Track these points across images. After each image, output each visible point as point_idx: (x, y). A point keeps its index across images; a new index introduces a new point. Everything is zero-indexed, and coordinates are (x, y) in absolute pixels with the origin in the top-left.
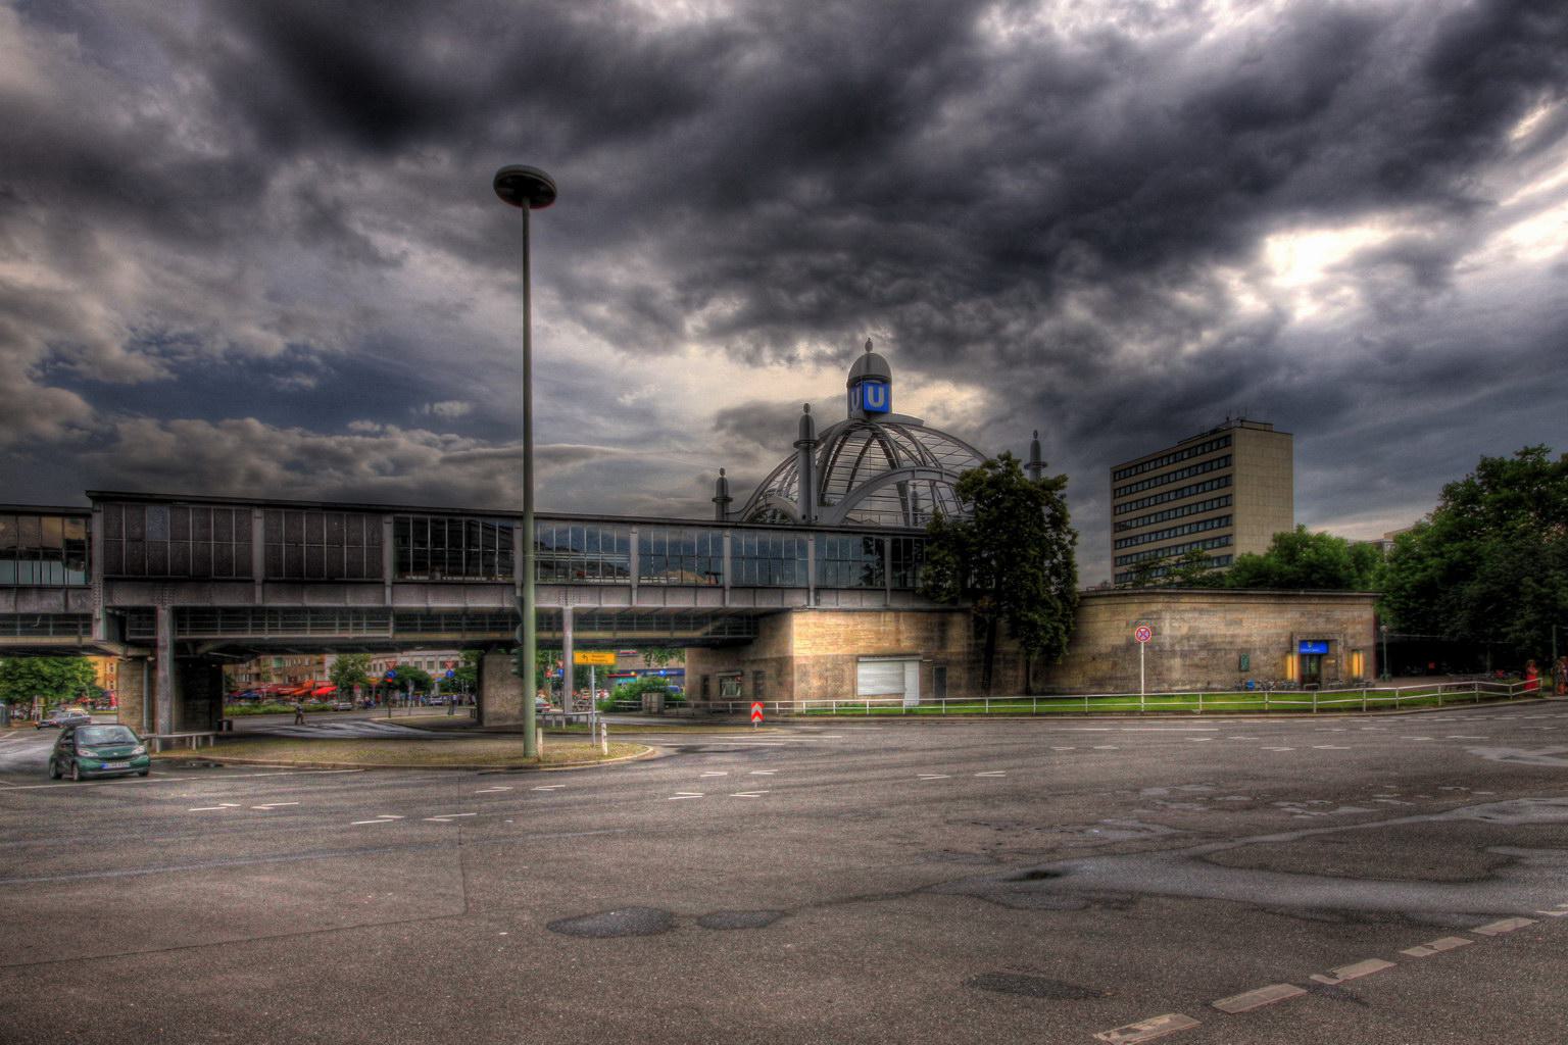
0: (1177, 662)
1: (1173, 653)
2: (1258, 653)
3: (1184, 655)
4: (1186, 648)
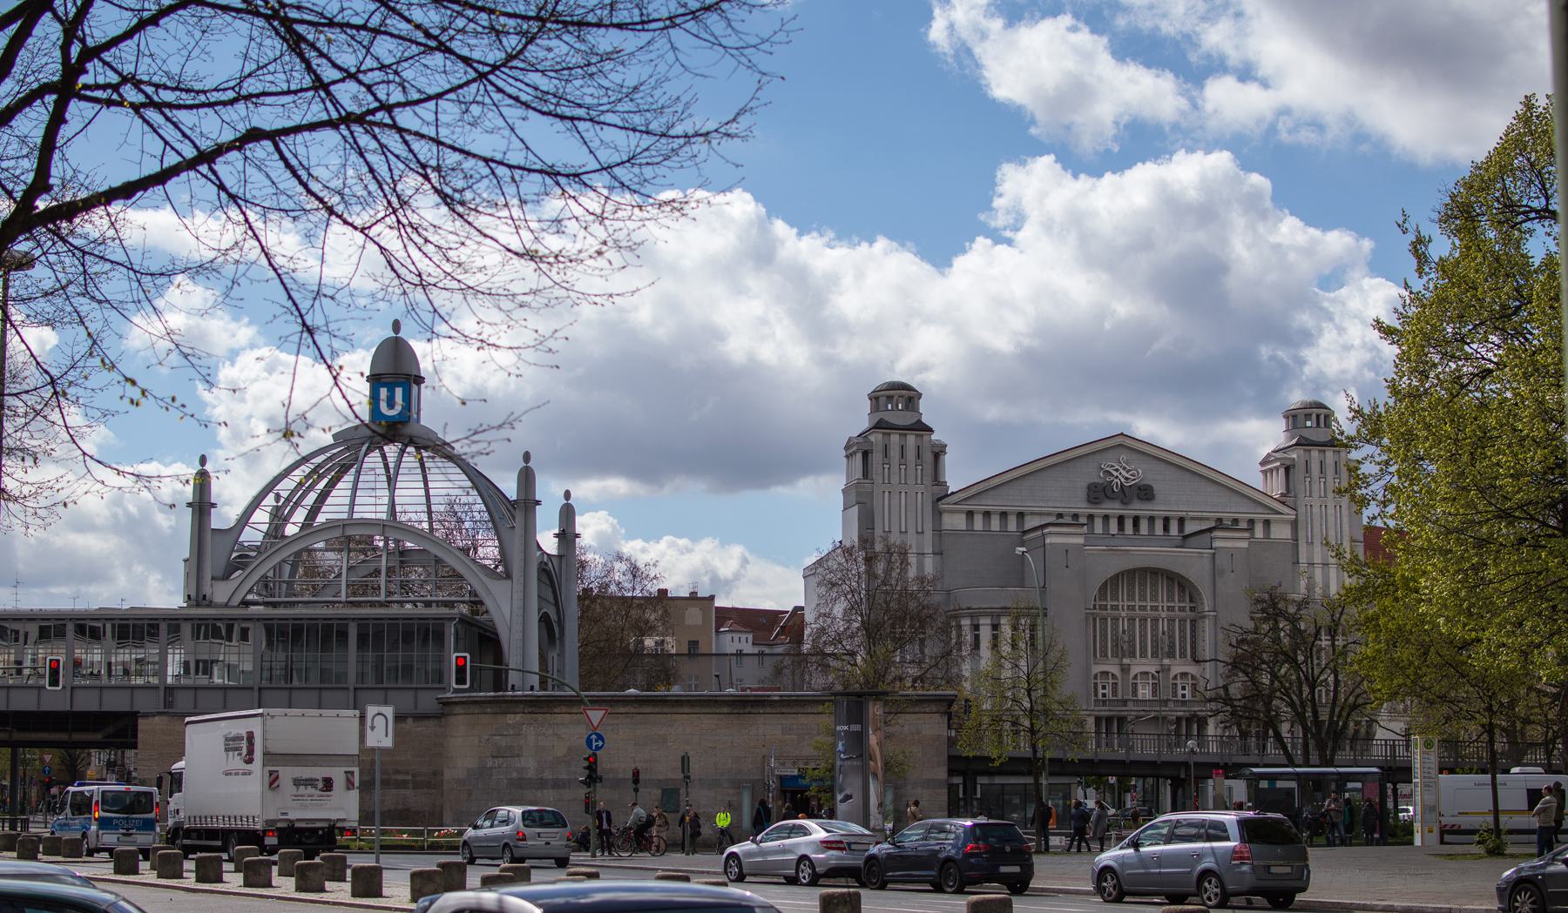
4: (564, 776)
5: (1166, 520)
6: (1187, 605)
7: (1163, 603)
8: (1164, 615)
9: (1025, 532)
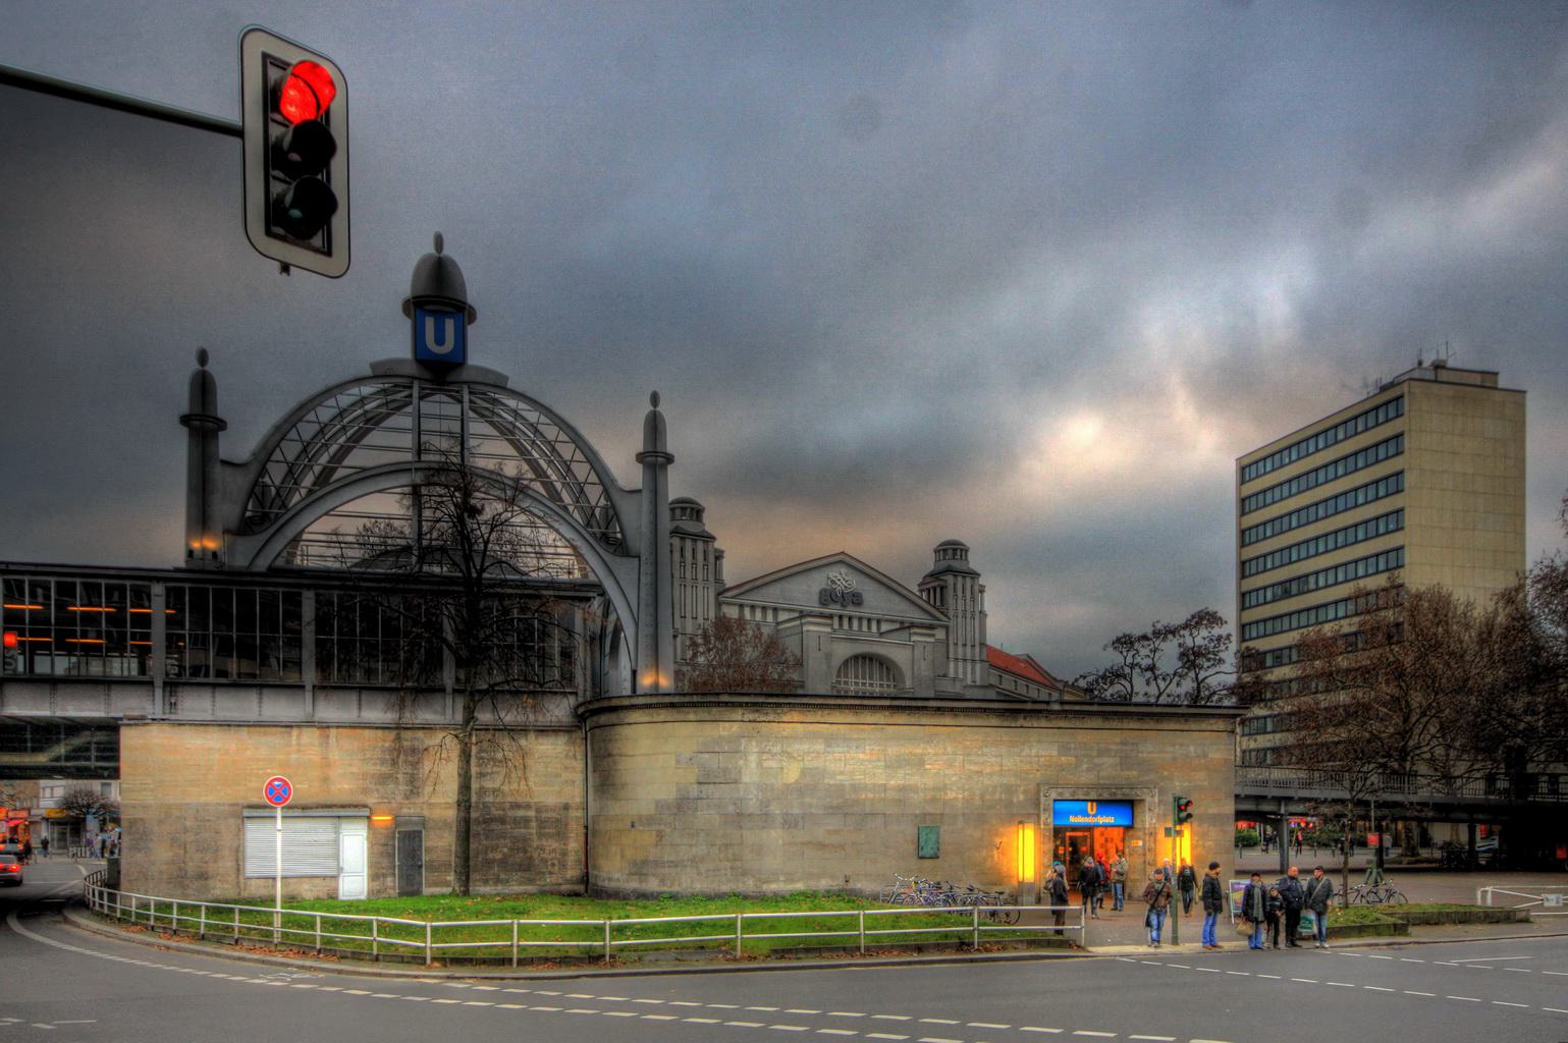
0: (775, 836)
1: (765, 819)
2: (960, 823)
3: (790, 823)
4: (796, 811)
6: (892, 683)
9: (778, 624)
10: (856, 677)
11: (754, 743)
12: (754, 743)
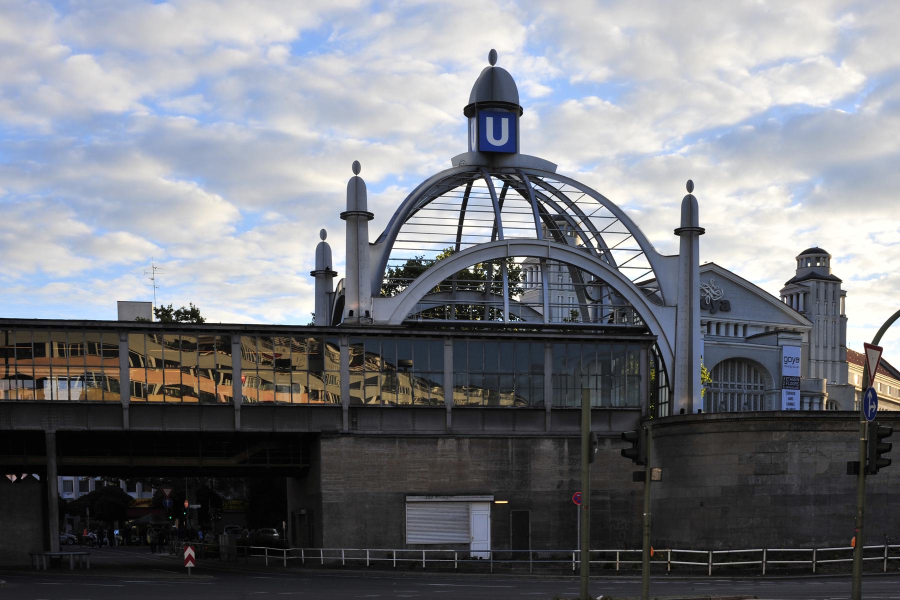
4: (825, 492)
5: (736, 326)
6: (759, 385)
7: (744, 383)
8: (745, 391)
10: (726, 379)
11: (797, 446)
12: (797, 446)
